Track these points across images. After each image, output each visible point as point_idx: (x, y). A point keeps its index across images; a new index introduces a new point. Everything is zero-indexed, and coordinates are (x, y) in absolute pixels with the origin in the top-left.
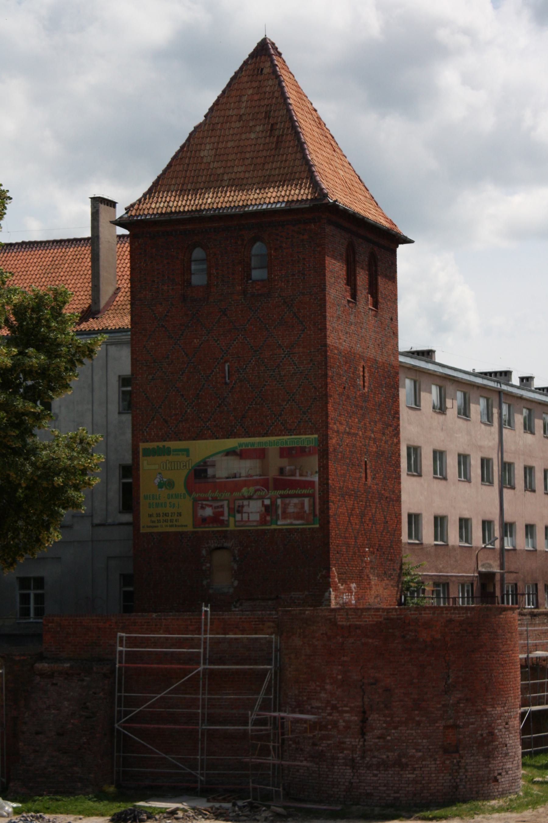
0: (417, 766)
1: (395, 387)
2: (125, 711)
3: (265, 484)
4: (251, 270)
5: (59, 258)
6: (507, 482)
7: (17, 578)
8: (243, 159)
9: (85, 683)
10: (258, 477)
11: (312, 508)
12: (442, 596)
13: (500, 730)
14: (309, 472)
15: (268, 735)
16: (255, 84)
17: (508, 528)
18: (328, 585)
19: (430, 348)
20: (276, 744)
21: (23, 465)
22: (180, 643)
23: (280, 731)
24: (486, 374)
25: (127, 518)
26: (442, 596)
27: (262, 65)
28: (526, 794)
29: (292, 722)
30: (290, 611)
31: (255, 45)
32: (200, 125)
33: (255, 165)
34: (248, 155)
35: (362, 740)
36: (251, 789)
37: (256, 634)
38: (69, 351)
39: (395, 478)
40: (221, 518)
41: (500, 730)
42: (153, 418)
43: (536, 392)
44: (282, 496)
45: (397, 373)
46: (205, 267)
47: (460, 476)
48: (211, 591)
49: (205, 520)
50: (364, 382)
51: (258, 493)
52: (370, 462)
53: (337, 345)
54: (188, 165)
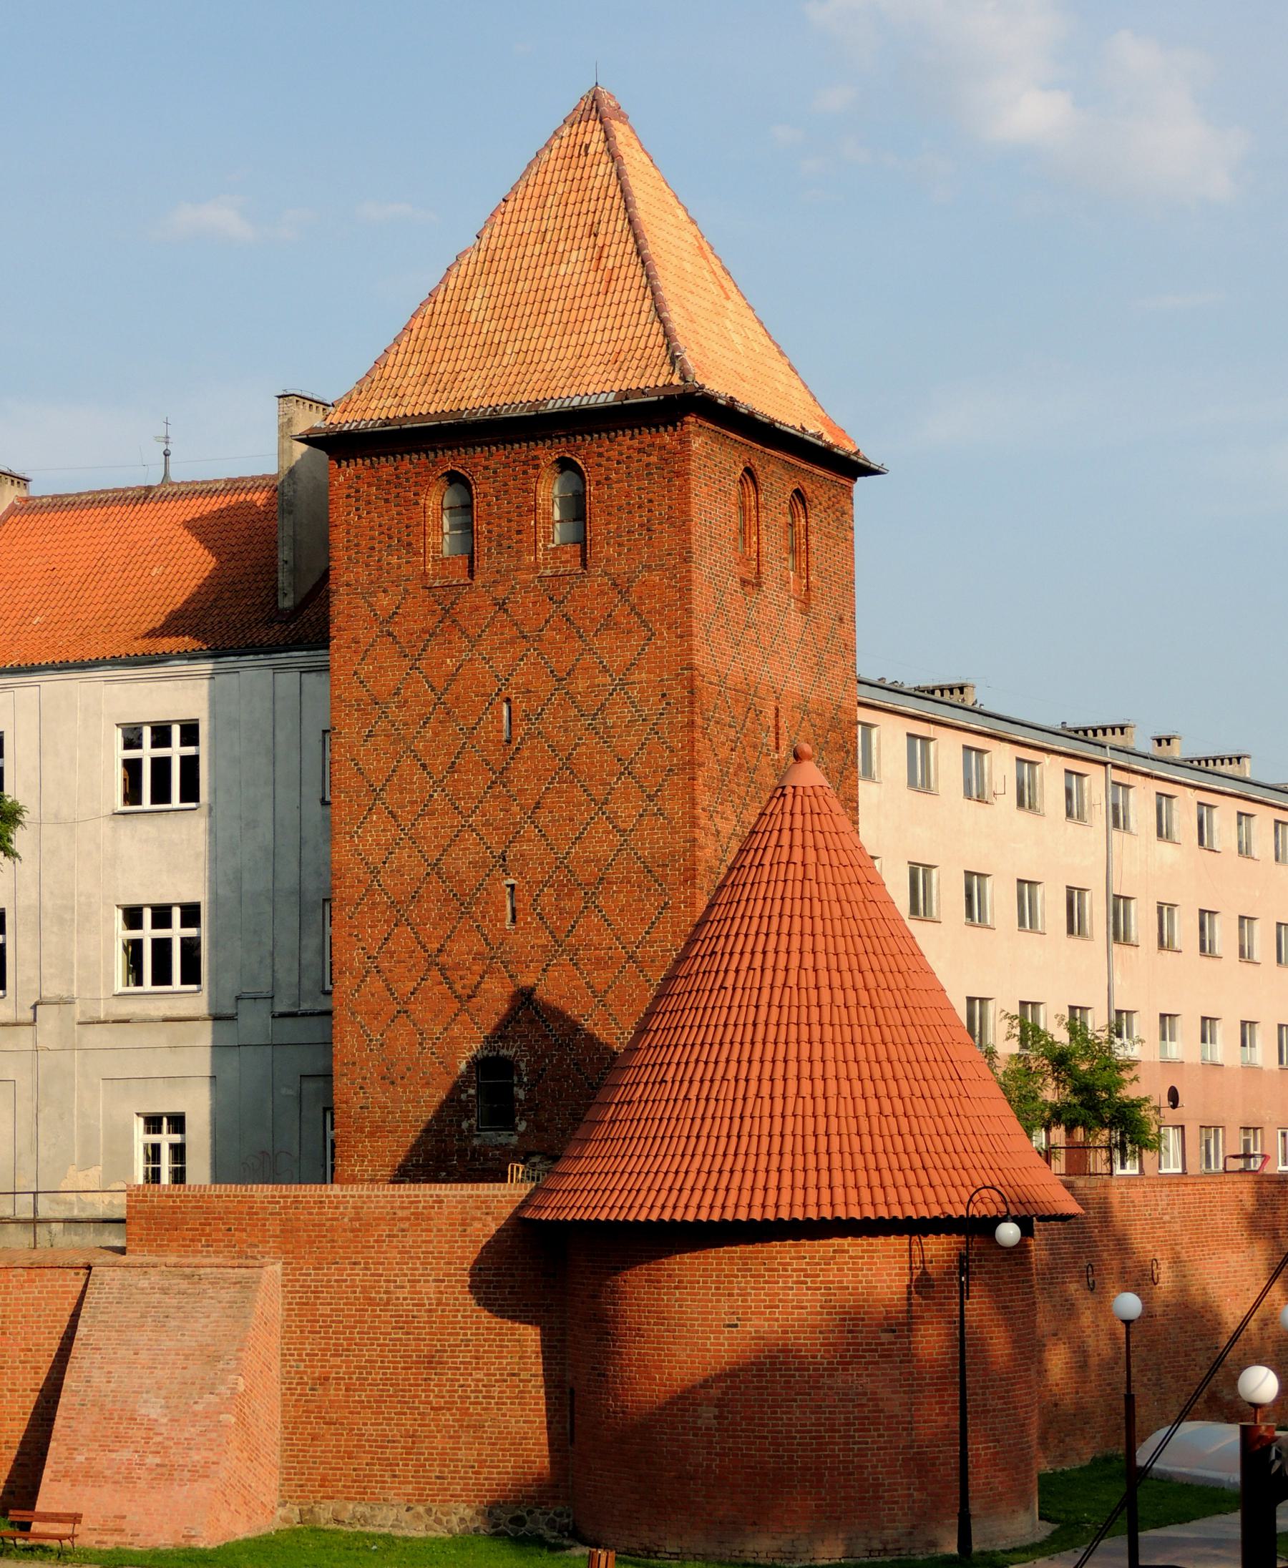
42: (370, 809)
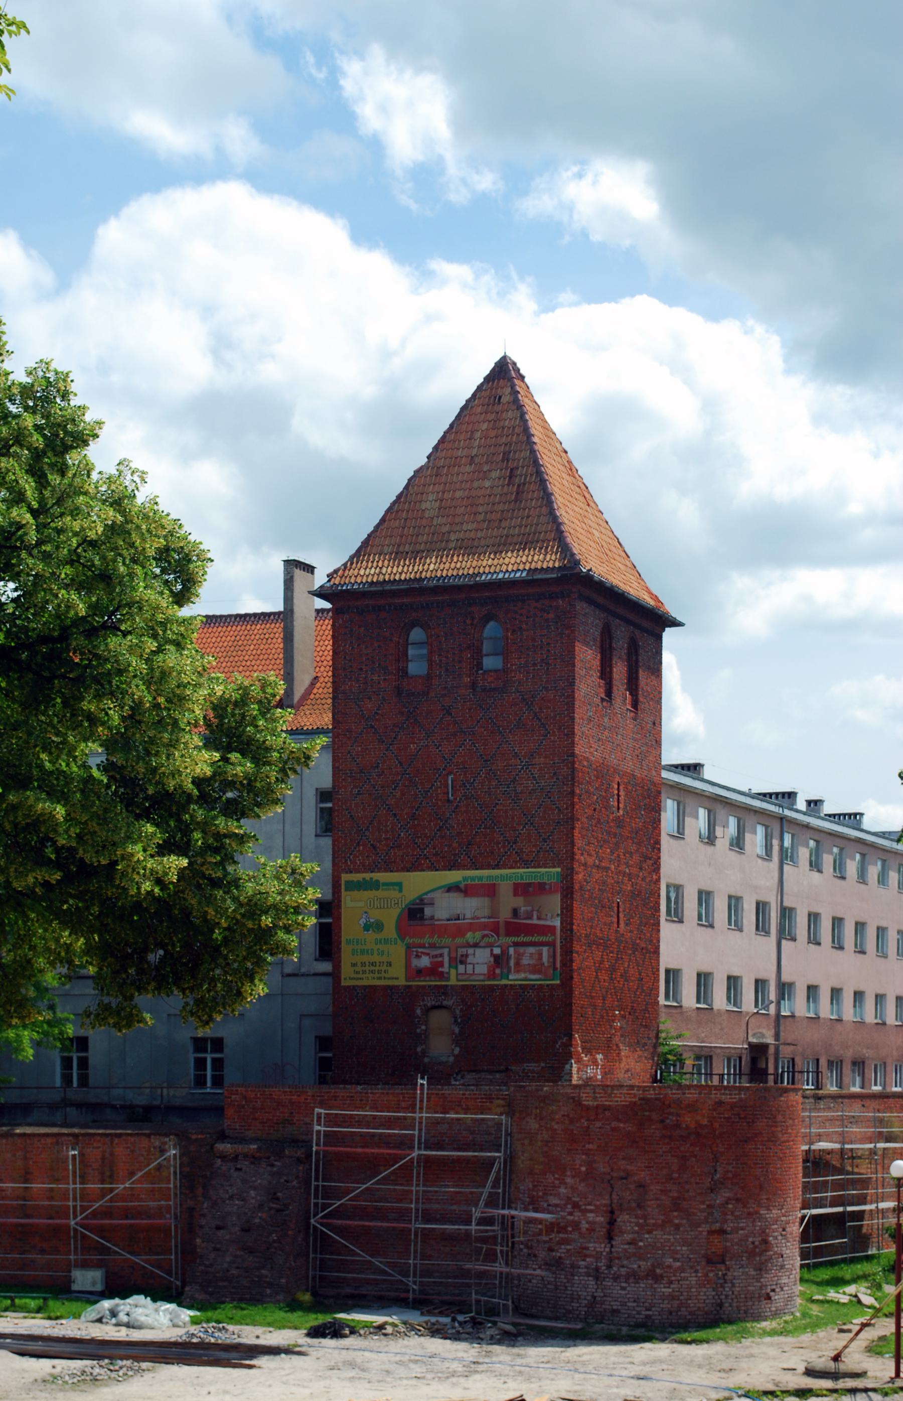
0: (673, 1278)
1: (656, 809)
2: (323, 1204)
3: (495, 928)
4: (482, 657)
5: (243, 638)
6: (786, 933)
7: (191, 1038)
8: (475, 514)
9: (275, 1169)
10: (486, 920)
11: (551, 960)
12: (703, 1071)
13: (776, 1238)
14: (549, 915)
15: (495, 1237)
16: (491, 417)
17: (785, 989)
18: (569, 1055)
19: (697, 762)
20: (505, 1249)
21: (224, 900)
22: (389, 1123)
23: (510, 1233)
24: (765, 795)
25: (325, 967)
26: (703, 1071)
27: (499, 392)
28: (804, 1315)
29: (524, 1222)
30: (524, 1087)
31: (492, 365)
32: (422, 467)
33: (489, 521)
34: (480, 509)
35: (609, 1245)
36: (474, 1302)
37: (482, 1113)
38: (281, 757)
39: (654, 925)
40: (440, 969)
41: (776, 1238)
43: (826, 820)
44: (516, 944)
45: (659, 793)
46: (425, 651)
47: (730, 924)
48: (426, 1060)
49: (420, 972)
50: (618, 803)
51: (486, 940)
52: (624, 903)
53: (588, 755)
54: (406, 520)
